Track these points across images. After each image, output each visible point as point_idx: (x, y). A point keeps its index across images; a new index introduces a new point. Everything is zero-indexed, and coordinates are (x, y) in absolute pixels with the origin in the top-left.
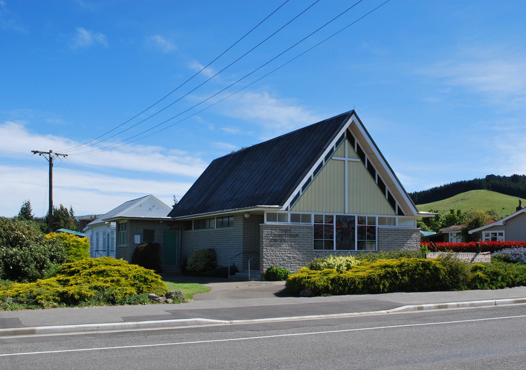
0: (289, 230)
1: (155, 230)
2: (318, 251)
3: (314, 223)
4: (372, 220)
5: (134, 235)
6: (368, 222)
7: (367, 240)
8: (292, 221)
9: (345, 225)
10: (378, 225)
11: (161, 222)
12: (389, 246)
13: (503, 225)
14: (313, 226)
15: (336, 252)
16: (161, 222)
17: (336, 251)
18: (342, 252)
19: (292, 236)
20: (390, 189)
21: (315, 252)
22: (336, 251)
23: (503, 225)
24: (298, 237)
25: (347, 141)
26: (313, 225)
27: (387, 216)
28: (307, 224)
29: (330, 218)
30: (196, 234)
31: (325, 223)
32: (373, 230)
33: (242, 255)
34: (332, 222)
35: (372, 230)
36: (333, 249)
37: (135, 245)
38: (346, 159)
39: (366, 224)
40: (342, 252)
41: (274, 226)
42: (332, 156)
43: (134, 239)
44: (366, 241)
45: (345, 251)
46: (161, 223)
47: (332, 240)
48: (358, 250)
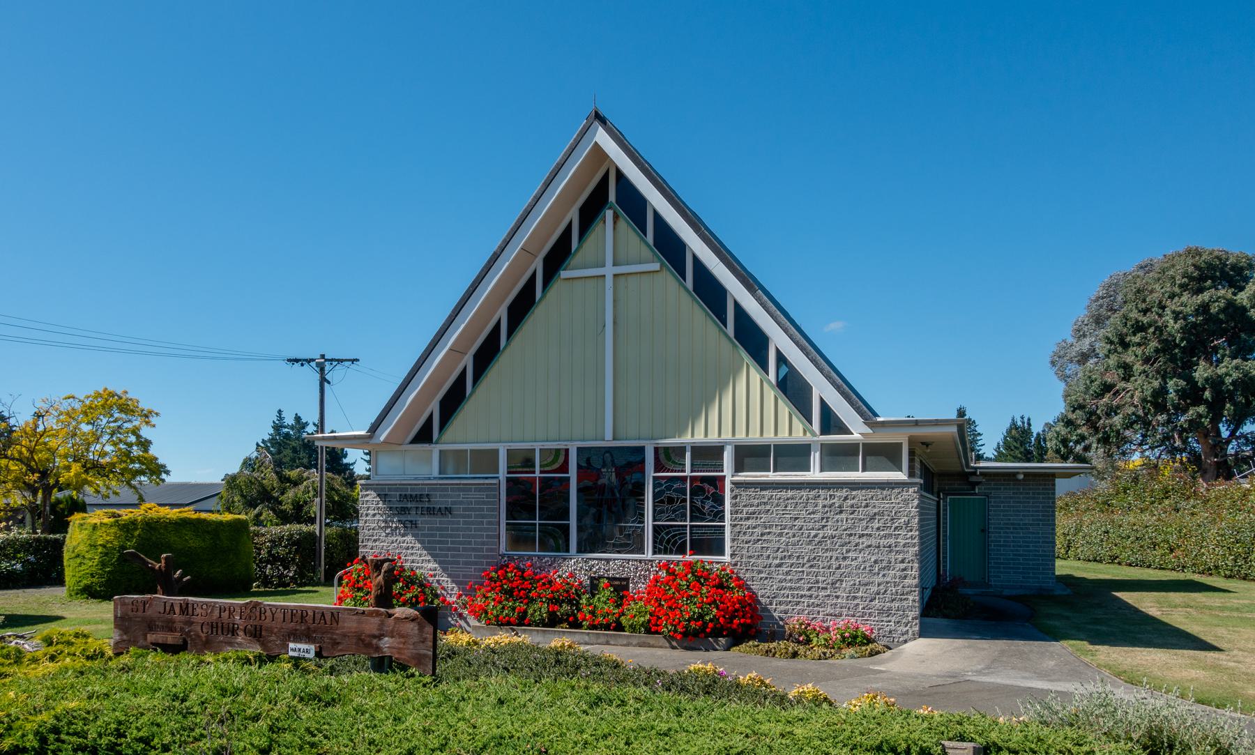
0: (428, 495)
3: (509, 473)
6: (541, 466)
28: (486, 478)
39: (534, 472)
47: (565, 524)
48: (654, 553)
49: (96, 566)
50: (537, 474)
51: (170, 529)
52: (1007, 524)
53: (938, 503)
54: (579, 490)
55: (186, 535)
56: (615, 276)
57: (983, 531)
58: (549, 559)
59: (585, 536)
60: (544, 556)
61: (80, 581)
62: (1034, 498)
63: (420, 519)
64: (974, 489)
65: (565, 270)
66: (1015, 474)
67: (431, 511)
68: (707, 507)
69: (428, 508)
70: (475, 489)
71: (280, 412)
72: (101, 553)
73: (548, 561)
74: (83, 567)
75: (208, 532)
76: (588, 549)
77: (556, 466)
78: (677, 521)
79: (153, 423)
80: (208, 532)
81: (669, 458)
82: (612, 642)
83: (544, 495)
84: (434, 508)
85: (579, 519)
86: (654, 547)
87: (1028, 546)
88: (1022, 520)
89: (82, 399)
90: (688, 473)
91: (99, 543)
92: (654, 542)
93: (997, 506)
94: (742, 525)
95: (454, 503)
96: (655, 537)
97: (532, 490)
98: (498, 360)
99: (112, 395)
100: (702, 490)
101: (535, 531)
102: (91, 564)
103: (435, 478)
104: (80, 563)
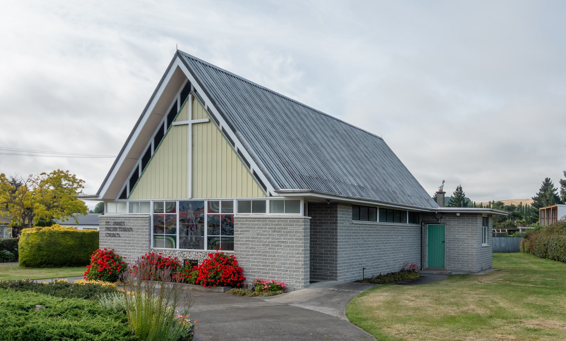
0: (123, 222)
3: (154, 212)
4: (228, 205)
6: (166, 210)
7: (220, 236)
11: (458, 215)
12: (248, 244)
29: (171, 206)
30: (396, 228)
31: (166, 212)
32: (229, 221)
34: (174, 211)
38: (190, 122)
39: (163, 212)
41: (277, 220)
46: (457, 216)
47: (175, 235)
48: (208, 249)
49: (28, 252)
51: (60, 236)
52: (454, 238)
53: (422, 227)
54: (180, 221)
55: (67, 239)
56: (193, 124)
57: (443, 242)
61: (22, 259)
62: (467, 225)
64: (438, 221)
65: (175, 121)
66: (455, 213)
67: (125, 230)
69: (123, 228)
70: (141, 219)
72: (30, 247)
74: (24, 253)
75: (78, 238)
77: (211, 208)
79: (83, 186)
80: (78, 238)
81: (213, 207)
83: (167, 223)
84: (126, 228)
85: (180, 234)
86: (208, 246)
87: (464, 250)
88: (461, 236)
89: (49, 174)
90: (220, 213)
91: (30, 242)
92: (208, 244)
93: (450, 230)
95: (133, 226)
97: (163, 221)
98: (150, 162)
99: (62, 172)
100: (225, 220)
102: (26, 251)
103: (127, 214)
104: (23, 251)
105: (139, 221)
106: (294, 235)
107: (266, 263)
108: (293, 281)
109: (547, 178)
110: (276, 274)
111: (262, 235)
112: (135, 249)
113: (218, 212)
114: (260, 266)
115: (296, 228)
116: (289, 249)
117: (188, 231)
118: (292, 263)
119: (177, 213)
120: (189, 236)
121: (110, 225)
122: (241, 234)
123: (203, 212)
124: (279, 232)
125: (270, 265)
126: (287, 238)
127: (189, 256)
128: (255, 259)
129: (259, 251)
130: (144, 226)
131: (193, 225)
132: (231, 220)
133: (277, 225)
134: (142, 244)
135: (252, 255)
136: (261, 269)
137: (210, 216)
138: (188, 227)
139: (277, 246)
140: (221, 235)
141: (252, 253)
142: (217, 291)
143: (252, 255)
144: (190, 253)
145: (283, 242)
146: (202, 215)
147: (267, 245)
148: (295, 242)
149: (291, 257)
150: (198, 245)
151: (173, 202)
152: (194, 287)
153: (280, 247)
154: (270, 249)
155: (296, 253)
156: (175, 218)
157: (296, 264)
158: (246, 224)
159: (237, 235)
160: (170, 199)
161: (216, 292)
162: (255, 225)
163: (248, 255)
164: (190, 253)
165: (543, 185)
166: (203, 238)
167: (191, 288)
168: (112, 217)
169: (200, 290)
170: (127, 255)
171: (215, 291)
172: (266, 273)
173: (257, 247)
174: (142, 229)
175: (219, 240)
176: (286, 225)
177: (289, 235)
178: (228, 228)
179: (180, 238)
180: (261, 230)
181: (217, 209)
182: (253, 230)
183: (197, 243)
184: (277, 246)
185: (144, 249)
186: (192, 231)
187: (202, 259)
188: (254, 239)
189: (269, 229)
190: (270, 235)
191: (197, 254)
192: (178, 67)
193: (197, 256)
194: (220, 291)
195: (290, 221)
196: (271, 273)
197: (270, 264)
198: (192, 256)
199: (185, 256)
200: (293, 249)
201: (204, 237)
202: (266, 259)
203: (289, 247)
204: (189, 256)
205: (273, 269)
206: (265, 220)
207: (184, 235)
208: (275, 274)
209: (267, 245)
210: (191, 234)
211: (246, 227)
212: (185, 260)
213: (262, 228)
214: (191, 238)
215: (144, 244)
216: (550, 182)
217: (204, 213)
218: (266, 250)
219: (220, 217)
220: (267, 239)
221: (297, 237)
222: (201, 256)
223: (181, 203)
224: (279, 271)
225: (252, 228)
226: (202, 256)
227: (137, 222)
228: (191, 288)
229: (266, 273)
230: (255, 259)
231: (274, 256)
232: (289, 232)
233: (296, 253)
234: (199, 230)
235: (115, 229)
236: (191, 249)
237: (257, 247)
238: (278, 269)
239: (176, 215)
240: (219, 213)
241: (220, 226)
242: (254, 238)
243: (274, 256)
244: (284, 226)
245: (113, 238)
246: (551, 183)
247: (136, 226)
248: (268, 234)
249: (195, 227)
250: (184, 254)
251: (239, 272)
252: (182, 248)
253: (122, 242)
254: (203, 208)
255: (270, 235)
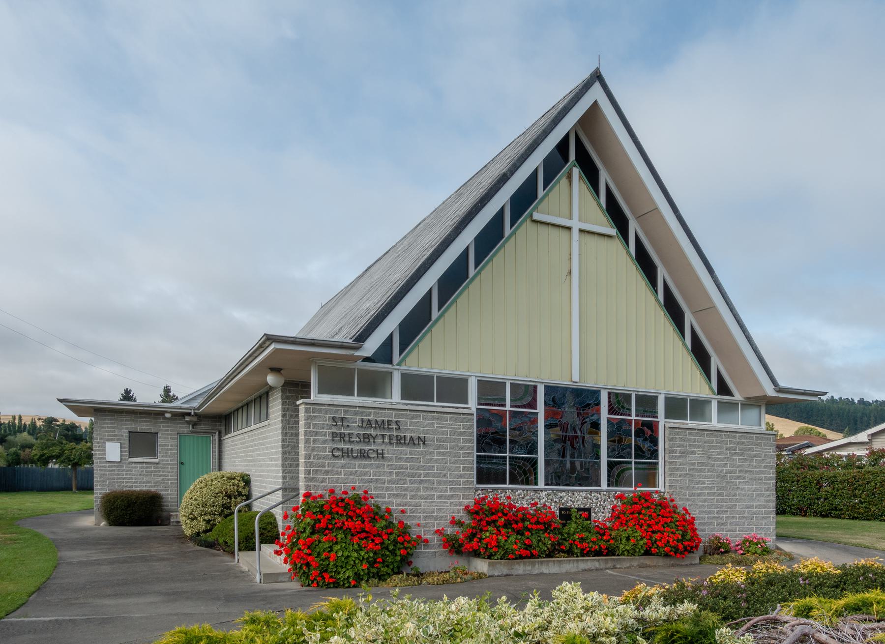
0: (397, 422)
1: (157, 433)
2: (490, 488)
3: (479, 404)
4: (647, 403)
5: (104, 443)
8: (405, 395)
9: (570, 414)
10: (666, 418)
11: (168, 415)
12: (693, 476)
13: (868, 441)
14: (472, 415)
15: (544, 493)
16: (168, 415)
17: (546, 490)
18: (564, 491)
19: (405, 443)
20: (698, 322)
21: (479, 492)
22: (546, 490)
23: (868, 441)
24: (424, 443)
25: (576, 171)
26: (474, 410)
27: (508, 486)
28: (457, 408)
33: (280, 492)
34: (533, 404)
35: (648, 432)
36: (536, 484)
37: (107, 465)
40: (564, 491)
41: (737, 435)
42: (533, 210)
43: (105, 451)
44: (631, 463)
45: (573, 491)
47: (534, 458)
48: (609, 485)
50: (508, 408)
58: (521, 491)
59: (551, 470)
60: (517, 490)
63: (386, 448)
68: (646, 447)
71: (61, 401)
73: (521, 494)
76: (554, 482)
78: (625, 458)
82: (618, 566)
85: (546, 455)
86: (609, 480)
92: (609, 476)
94: (676, 462)
96: (609, 472)
101: (506, 464)
105: (447, 420)
106: (763, 460)
107: (722, 507)
108: (761, 533)
109: (127, 389)
110: (738, 525)
111: (715, 459)
112: (432, 489)
113: (630, 415)
114: (713, 512)
115: (766, 449)
116: (756, 482)
117: (564, 450)
118: (760, 505)
119: (541, 409)
120: (568, 459)
121: (348, 426)
122: (680, 457)
123: (598, 412)
124: (741, 455)
125: (727, 511)
126: (752, 465)
127: (571, 500)
128: (705, 500)
129: (711, 488)
130: (461, 434)
131: (577, 437)
132: (652, 431)
133: (738, 443)
134: (455, 478)
135: (699, 495)
136: (714, 517)
137: (612, 420)
138: (565, 442)
139: (739, 477)
140: (634, 459)
141: (699, 491)
142: (689, 563)
143: (699, 495)
144: (573, 494)
145: (747, 472)
146: (595, 418)
147: (724, 477)
148: (764, 471)
149: (758, 495)
150: (588, 478)
151: (529, 385)
152: (642, 561)
153: (743, 480)
154: (727, 483)
155: (765, 488)
156: (535, 421)
157: (765, 507)
158: (690, 440)
159: (674, 459)
160: (523, 377)
161: (687, 565)
162: (705, 442)
163: (693, 494)
164: (573, 494)
165: (122, 398)
166: (599, 464)
167: (635, 564)
168: (356, 407)
169: (655, 566)
170: (406, 505)
171: (683, 563)
172: (723, 524)
173: (708, 481)
174: (454, 442)
175: (631, 469)
176: (751, 445)
177: (756, 460)
178: (646, 446)
179: (547, 463)
180: (714, 452)
181: (627, 409)
182: (702, 451)
183: (585, 475)
184: (739, 477)
185: (460, 489)
186: (575, 449)
187: (601, 505)
188: (703, 466)
189: (726, 449)
190: (728, 459)
191: (590, 496)
192: (595, 104)
193: (589, 500)
194: (693, 563)
195: (757, 438)
196: (730, 524)
197: (728, 508)
198: (578, 500)
199: (563, 501)
200: (761, 484)
201: (600, 462)
202: (723, 500)
203: (756, 480)
204: (571, 500)
205: (733, 517)
206: (720, 435)
207: (555, 457)
208: (735, 525)
209: (724, 477)
210: (572, 456)
211: (690, 445)
212: (561, 510)
213: (715, 448)
214: (573, 464)
215: (461, 476)
216: (131, 395)
217: (599, 414)
218: (723, 484)
219: (632, 423)
220: (724, 466)
221: (766, 463)
222: (598, 499)
223: (550, 390)
224: (741, 519)
225: (699, 447)
226: (600, 499)
227: (438, 424)
228: (635, 564)
229: (723, 524)
230: (705, 500)
231: (735, 495)
232: (755, 456)
233: (765, 488)
234: (588, 447)
235: (367, 438)
236: (573, 486)
237: (708, 481)
238: (739, 517)
239: (538, 413)
240: (631, 416)
241: (506, 443)
242: (703, 464)
243: (735, 495)
244: (749, 445)
245: (357, 462)
246: (132, 397)
247: (434, 433)
248: (725, 458)
249: (581, 442)
250: (561, 497)
251: (687, 524)
252: (552, 484)
253: (390, 472)
254: (598, 404)
255: (728, 459)
